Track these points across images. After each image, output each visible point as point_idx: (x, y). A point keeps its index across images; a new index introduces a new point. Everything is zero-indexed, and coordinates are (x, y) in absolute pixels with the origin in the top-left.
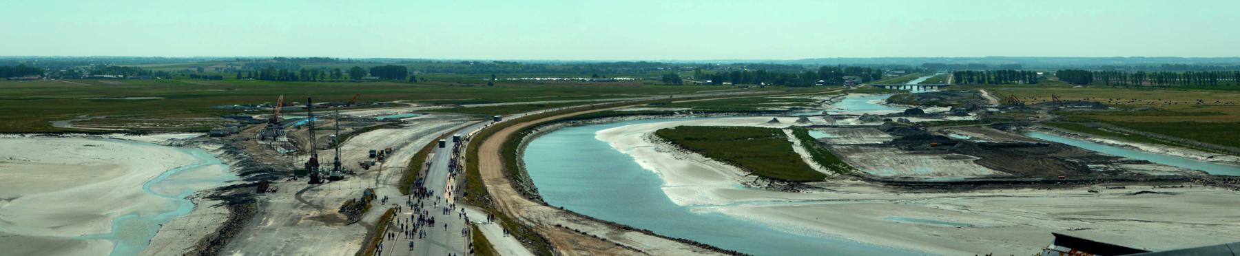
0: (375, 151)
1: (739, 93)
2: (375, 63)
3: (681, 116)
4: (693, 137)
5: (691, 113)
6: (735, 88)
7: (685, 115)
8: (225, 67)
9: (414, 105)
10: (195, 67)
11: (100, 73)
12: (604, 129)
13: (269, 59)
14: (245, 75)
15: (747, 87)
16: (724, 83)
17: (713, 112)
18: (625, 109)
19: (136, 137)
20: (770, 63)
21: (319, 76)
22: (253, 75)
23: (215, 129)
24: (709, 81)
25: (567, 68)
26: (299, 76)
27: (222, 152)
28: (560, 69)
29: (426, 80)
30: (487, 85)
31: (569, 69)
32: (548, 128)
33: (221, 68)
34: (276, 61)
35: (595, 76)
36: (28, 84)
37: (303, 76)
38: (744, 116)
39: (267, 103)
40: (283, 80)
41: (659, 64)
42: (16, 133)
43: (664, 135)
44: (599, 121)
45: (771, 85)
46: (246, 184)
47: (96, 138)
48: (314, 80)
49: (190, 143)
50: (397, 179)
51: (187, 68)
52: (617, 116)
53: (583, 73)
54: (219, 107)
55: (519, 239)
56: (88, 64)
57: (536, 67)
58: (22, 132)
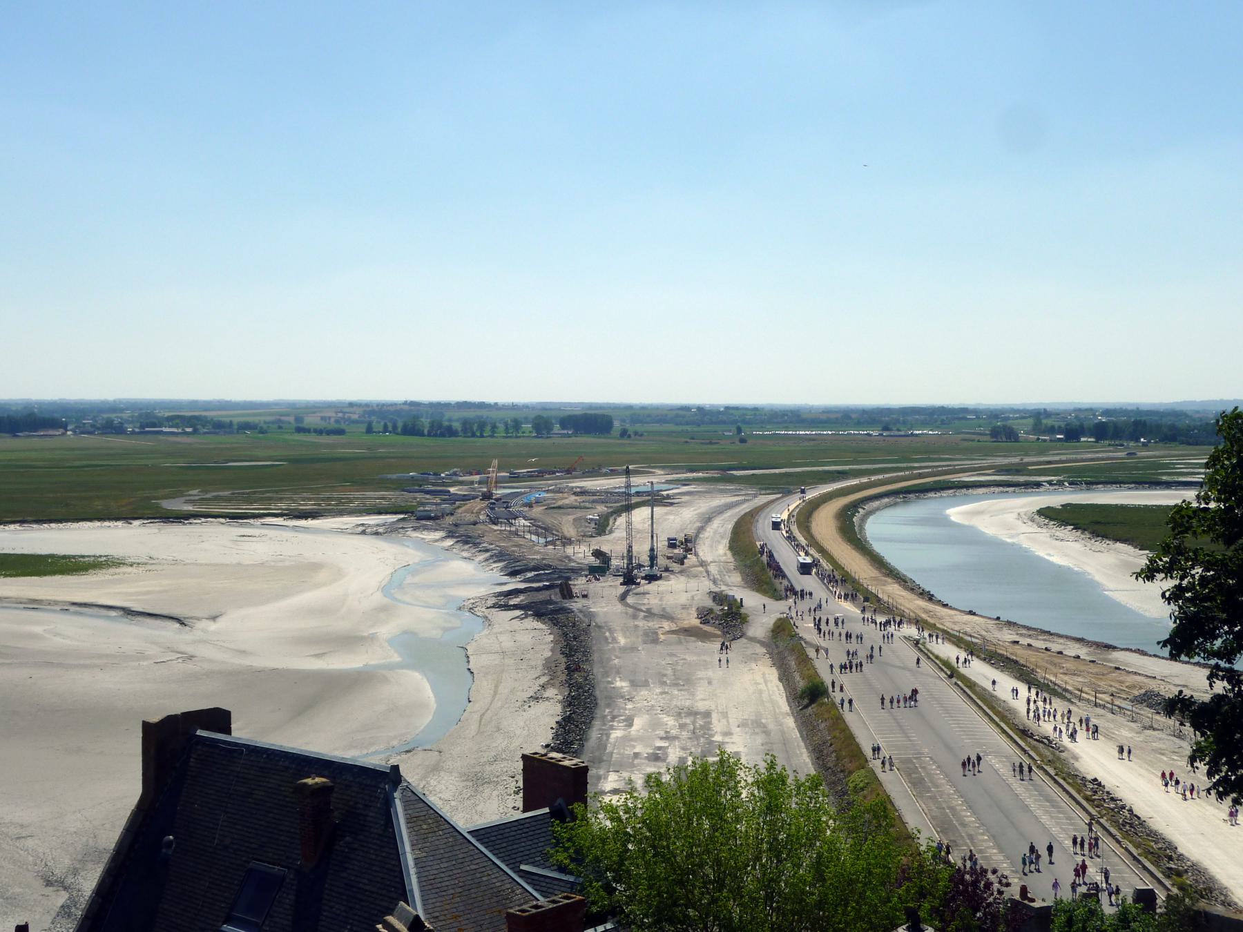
0: (675, 539)
1: (1111, 454)
2: (560, 409)
3: (1051, 488)
4: (1103, 520)
5: (1066, 484)
6: (1104, 447)
7: (1056, 487)
8: (333, 415)
9: (659, 472)
10: (288, 415)
11: (154, 425)
12: (958, 506)
13: (396, 404)
14: (378, 427)
15: (1122, 445)
16: (1082, 439)
17: (1097, 483)
18: (966, 478)
19: (302, 523)
20: (1134, 408)
21: (488, 428)
22: (390, 429)
24: (1058, 436)
25: (833, 416)
26: (460, 429)
27: (449, 542)
28: (824, 417)
29: (642, 435)
30: (738, 443)
31: (837, 419)
33: (330, 418)
34: (406, 407)
35: (886, 428)
36: (48, 443)
37: (465, 430)
38: (1144, 489)
39: (455, 470)
40: (435, 435)
41: (965, 410)
42: (117, 519)
43: (1048, 514)
44: (938, 494)
45: (1156, 442)
47: (242, 525)
48: (482, 436)
49: (391, 530)
51: (278, 417)
52: (961, 487)
53: (859, 424)
54: (389, 476)
55: (984, 660)
56: (122, 410)
58: (127, 518)
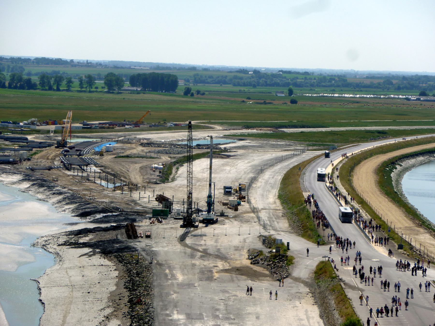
0: (230, 188)
9: (218, 127)
21: (64, 83)
26: (38, 83)
27: (26, 185)
28: (367, 82)
29: (203, 94)
32: (412, 161)
35: (423, 94)
37: (43, 84)
40: (16, 87)
46: (101, 228)
48: (58, 90)
50: (404, 247)
57: (334, 79)
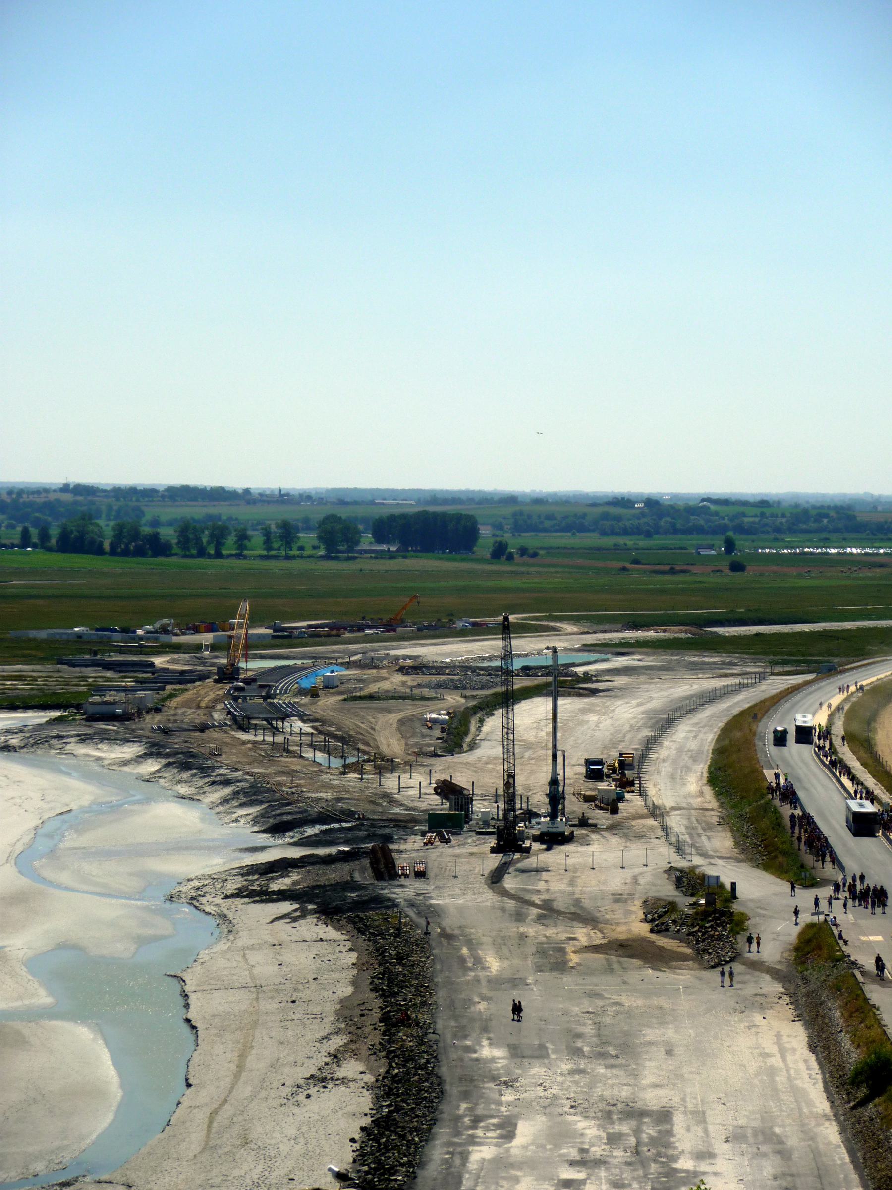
0: (600, 762)
2: (372, 503)
9: (569, 628)
13: (46, 491)
21: (231, 540)
22: (35, 540)
23: (97, 698)
26: (174, 541)
29: (535, 555)
34: (67, 497)
39: (165, 621)
40: (126, 553)
48: (218, 555)
54: (33, 634)
57: (826, 516)
